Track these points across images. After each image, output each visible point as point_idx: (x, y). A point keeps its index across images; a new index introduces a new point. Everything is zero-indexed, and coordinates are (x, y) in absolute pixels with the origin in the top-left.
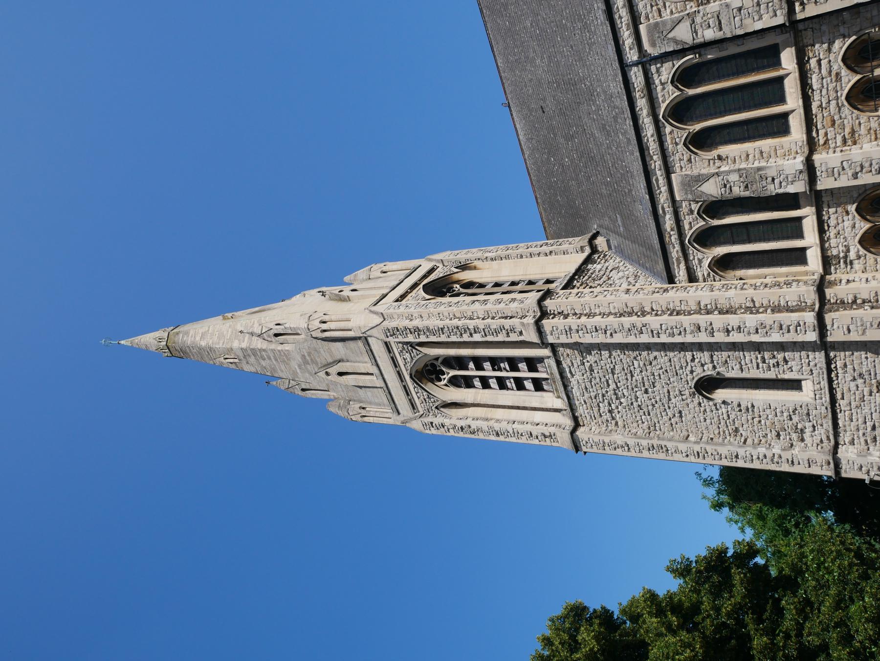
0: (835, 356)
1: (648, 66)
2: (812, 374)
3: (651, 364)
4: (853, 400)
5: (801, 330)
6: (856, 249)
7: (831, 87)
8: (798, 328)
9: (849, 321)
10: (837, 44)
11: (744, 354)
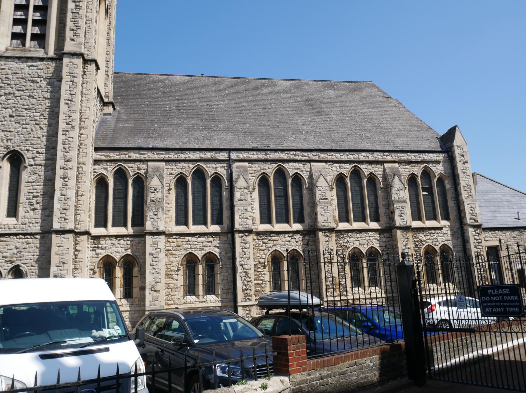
0: (36, 238)
1: (227, 162)
2: (22, 224)
3: (37, 124)
5: (62, 220)
6: (103, 253)
7: (198, 246)
8: (63, 219)
9: (66, 246)
10: (217, 250)
11: (41, 185)
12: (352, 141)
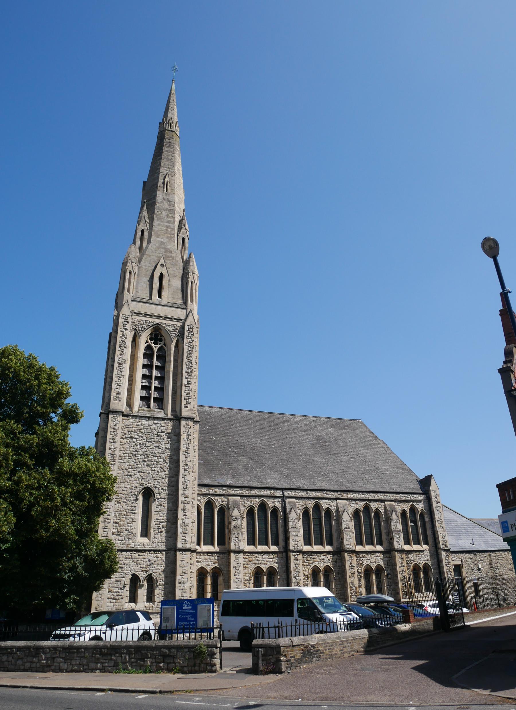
0: (162, 554)
2: (153, 543)
3: (161, 468)
4: (138, 559)
7: (263, 562)
12: (361, 482)
